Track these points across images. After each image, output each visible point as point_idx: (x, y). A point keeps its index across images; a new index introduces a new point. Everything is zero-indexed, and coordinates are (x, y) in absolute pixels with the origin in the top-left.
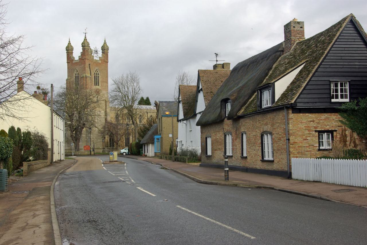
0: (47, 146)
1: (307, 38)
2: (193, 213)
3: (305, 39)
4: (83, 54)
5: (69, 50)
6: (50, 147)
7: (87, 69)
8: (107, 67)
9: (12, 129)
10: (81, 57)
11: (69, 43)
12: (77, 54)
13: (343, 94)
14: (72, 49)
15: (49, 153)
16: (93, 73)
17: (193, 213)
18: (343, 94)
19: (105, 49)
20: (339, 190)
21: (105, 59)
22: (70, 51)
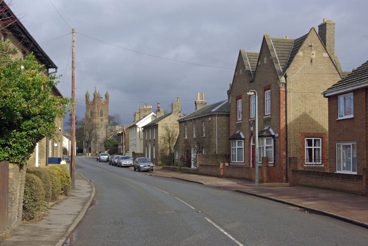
0: (67, 151)
1: (57, 87)
2: (233, 239)
3: (207, 105)
4: (94, 99)
5: (87, 96)
6: (68, 151)
7: (96, 108)
8: (108, 106)
9: (37, 145)
10: (93, 101)
11: (87, 92)
12: (91, 98)
13: (312, 149)
14: (89, 96)
15: (68, 153)
16: (99, 110)
17: (233, 239)
18: (312, 149)
19: (107, 96)
20: (274, 187)
21: (107, 102)
22: (87, 97)
